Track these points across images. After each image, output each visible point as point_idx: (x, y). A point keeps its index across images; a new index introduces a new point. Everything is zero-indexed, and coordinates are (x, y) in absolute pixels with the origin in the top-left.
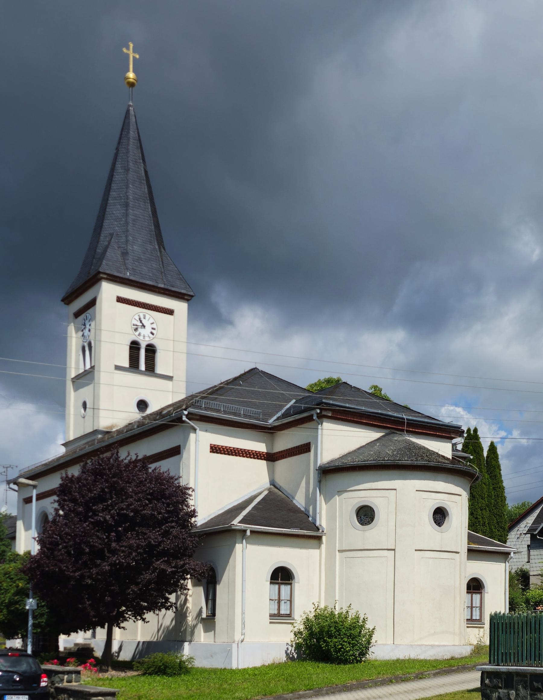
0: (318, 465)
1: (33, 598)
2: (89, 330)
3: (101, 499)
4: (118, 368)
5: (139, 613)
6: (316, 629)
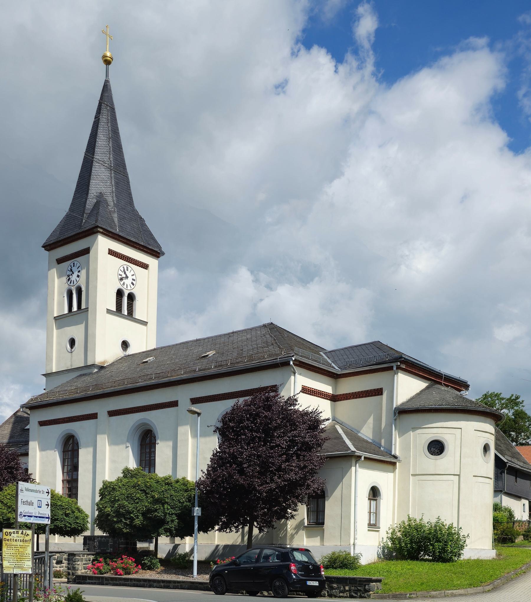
0: (395, 406)
1: (199, 507)
2: (78, 276)
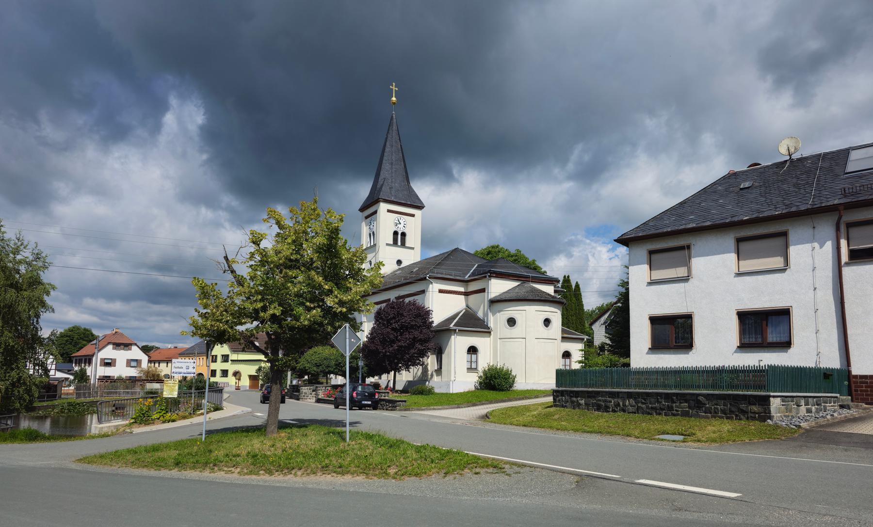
3: (394, 318)
4: (387, 244)
5: (407, 369)
6: (489, 375)
